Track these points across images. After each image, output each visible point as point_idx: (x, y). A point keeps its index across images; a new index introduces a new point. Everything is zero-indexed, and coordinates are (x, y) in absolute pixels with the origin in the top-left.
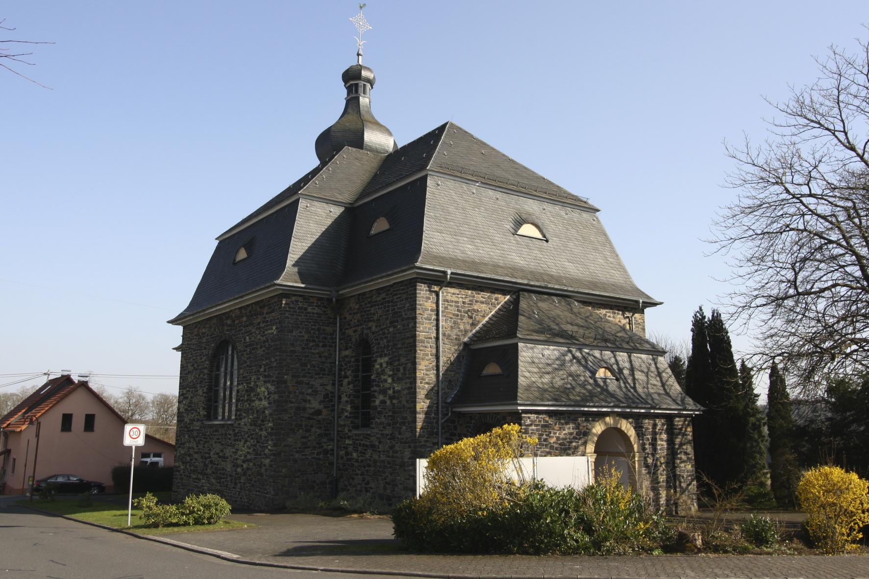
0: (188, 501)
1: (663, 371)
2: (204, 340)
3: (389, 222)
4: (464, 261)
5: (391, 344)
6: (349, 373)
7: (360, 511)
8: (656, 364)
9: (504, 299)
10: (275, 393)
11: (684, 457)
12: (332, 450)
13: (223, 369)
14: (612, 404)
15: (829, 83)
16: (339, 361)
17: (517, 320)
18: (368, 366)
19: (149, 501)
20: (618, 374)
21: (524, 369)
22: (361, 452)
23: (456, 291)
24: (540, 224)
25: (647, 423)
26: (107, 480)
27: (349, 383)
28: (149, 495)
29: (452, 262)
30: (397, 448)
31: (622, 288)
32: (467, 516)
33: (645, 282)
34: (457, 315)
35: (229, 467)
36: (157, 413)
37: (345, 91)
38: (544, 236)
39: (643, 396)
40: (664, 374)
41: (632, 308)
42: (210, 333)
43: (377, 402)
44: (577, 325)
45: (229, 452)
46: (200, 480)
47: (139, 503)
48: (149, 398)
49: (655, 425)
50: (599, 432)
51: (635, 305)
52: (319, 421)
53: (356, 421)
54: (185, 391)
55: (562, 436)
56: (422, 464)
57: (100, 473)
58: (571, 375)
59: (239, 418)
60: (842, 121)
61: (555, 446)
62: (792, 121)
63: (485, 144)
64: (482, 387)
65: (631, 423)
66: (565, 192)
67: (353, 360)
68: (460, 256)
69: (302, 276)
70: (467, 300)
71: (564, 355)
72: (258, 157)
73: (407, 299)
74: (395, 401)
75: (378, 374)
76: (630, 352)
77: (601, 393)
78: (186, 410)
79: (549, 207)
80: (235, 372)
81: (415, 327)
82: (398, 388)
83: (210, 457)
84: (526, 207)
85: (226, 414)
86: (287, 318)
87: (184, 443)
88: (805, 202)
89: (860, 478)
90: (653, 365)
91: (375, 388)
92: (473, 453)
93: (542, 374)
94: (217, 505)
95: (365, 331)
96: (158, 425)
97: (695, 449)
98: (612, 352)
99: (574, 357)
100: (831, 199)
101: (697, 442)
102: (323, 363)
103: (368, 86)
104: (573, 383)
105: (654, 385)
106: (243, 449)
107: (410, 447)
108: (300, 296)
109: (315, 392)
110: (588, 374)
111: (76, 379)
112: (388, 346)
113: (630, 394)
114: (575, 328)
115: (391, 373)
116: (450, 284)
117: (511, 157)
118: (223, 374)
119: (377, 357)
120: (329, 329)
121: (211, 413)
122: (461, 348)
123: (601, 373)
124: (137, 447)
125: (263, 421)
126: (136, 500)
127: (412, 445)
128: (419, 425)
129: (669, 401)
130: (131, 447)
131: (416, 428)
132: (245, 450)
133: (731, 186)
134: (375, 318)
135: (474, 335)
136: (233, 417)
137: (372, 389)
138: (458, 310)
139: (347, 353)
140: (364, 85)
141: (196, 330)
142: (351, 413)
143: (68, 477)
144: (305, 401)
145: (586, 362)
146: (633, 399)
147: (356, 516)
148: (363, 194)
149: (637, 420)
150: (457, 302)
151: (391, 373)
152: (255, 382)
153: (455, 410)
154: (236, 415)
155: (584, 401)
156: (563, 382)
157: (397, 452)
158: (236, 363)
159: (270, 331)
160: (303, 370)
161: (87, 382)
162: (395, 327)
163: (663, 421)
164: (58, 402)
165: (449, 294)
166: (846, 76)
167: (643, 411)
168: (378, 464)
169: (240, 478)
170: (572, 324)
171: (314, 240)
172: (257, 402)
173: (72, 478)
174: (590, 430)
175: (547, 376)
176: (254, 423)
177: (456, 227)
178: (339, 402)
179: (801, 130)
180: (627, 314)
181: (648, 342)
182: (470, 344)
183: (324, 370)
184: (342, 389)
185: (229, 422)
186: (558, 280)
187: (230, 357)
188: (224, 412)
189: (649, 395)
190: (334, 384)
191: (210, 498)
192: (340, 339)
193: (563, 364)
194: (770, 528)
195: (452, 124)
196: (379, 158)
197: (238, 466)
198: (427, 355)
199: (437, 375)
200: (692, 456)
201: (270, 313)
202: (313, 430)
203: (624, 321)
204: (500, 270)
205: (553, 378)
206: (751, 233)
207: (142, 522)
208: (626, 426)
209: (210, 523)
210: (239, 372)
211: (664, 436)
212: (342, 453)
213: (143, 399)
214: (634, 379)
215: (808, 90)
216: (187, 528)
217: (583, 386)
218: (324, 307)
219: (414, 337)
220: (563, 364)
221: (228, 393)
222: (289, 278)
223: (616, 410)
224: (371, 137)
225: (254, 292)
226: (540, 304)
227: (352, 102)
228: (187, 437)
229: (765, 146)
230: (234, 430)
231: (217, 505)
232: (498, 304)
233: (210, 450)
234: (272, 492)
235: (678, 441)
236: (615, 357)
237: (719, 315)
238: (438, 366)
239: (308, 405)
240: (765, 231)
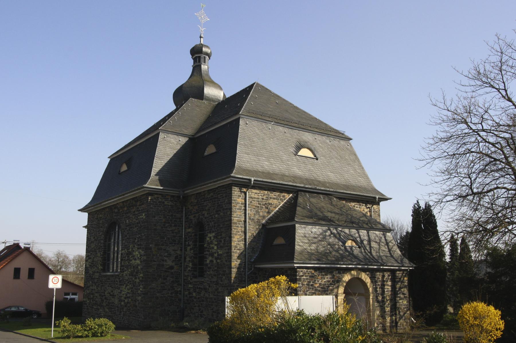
0: (88, 322)
1: (390, 242)
2: (101, 222)
3: (216, 147)
4: (263, 173)
5: (216, 225)
6: (191, 243)
7: (196, 329)
8: (385, 237)
9: (288, 197)
10: (144, 255)
11: (402, 296)
12: (181, 291)
13: (112, 240)
14: (355, 263)
15: (495, 59)
16: (185, 236)
17: (295, 210)
18: (202, 238)
19: (65, 322)
20: (360, 244)
21: (299, 241)
22: (198, 293)
23: (258, 191)
24: (313, 149)
25: (379, 275)
26: (43, 310)
27: (191, 249)
28: (65, 318)
29: (255, 173)
30: (220, 290)
31: (365, 189)
32: (253, 332)
33: (381, 185)
34: (258, 207)
35: (116, 301)
36: (76, 267)
37: (192, 61)
38: (315, 156)
39: (376, 257)
40: (390, 244)
41: (372, 202)
42: (105, 216)
43: (208, 262)
44: (334, 213)
45: (116, 292)
46: (99, 309)
47: (59, 323)
48: (71, 257)
49: (383, 276)
50: (347, 280)
51: (374, 200)
54: (89, 254)
55: (323, 283)
56: (228, 299)
57: (36, 305)
58: (329, 244)
59: (122, 271)
60: (504, 83)
61: (319, 289)
62: (472, 83)
63: (279, 97)
64: (273, 252)
65: (367, 275)
66: (331, 128)
67: (193, 235)
68: (260, 169)
69: (162, 182)
70: (264, 197)
71: (325, 232)
72: (136, 105)
73: (226, 196)
74: (218, 261)
75: (209, 244)
76: (368, 230)
77: (348, 256)
78: (90, 266)
79: (319, 137)
80: (120, 242)
81: (231, 214)
82: (220, 252)
83: (105, 296)
84: (304, 138)
85: (115, 268)
86: (152, 208)
88: (481, 135)
89: (496, 309)
90: (383, 238)
91: (207, 252)
92: (256, 293)
93: (311, 243)
94: (106, 325)
95: (201, 217)
96: (77, 274)
97: (409, 291)
98: (357, 230)
99: (332, 233)
100: (496, 133)
101: (411, 287)
103: (207, 58)
104: (331, 249)
105: (384, 251)
106: (125, 290)
107: (227, 289)
110: (341, 243)
111: (22, 246)
112: (215, 226)
113: (367, 256)
114: (333, 215)
115: (216, 243)
116: (254, 187)
117: (295, 105)
118: (112, 243)
119: (208, 233)
121: (106, 267)
122: (261, 227)
123: (349, 243)
124: (57, 289)
125: (137, 273)
126: (58, 322)
127: (229, 288)
128: (233, 275)
129: (392, 260)
130: (53, 289)
131: (231, 278)
133: (435, 124)
134: (207, 208)
135: (269, 219)
136: (119, 271)
137: (205, 253)
138: (259, 204)
139: (190, 230)
140: (205, 57)
142: (192, 268)
143: (18, 307)
144: (163, 261)
145: (340, 236)
146: (369, 259)
147: (193, 332)
148: (200, 129)
149: (372, 273)
150: (258, 198)
151: (216, 243)
152: (132, 249)
153: (256, 266)
154: (120, 269)
155: (337, 260)
156: (324, 249)
158: (120, 237)
159: (141, 217)
161: (29, 248)
162: (218, 214)
163: (389, 273)
164: (9, 262)
165: (253, 193)
166: (506, 54)
167: (375, 267)
168: (208, 300)
170: (331, 212)
171: (169, 159)
172: (133, 261)
173: (20, 308)
174: (341, 279)
175: (314, 245)
176: (131, 274)
177: (258, 150)
179: (478, 88)
180: (369, 206)
181: (380, 223)
182: (266, 225)
185: (117, 274)
186: (323, 184)
187: (117, 233)
188: (113, 267)
189: (380, 257)
190: (181, 250)
191: (103, 321)
192: (185, 222)
193: (324, 238)
194: (443, 340)
195: (258, 84)
196: (212, 106)
197: (122, 301)
198: (239, 232)
199: (245, 245)
200: (407, 295)
201: (141, 205)
202: (168, 278)
203: (366, 210)
204: (285, 178)
205: (318, 246)
206: (446, 154)
207: (60, 335)
208: (365, 277)
209: (102, 336)
210: (122, 242)
211: (389, 283)
212: (187, 293)
213: (67, 258)
214: (370, 247)
215: (483, 63)
216: (87, 338)
217: (337, 251)
219: (231, 220)
220: (324, 238)
221: (116, 255)
222: (153, 183)
223: (358, 266)
224: (208, 91)
225: (131, 192)
226: (312, 200)
227: (197, 68)
228: (91, 282)
229: (455, 99)
230: (119, 279)
231: (106, 325)
232: (284, 199)
233: (105, 291)
234: (143, 317)
235: (398, 286)
236: (358, 233)
238: (245, 239)
239: (165, 263)
240: (456, 153)
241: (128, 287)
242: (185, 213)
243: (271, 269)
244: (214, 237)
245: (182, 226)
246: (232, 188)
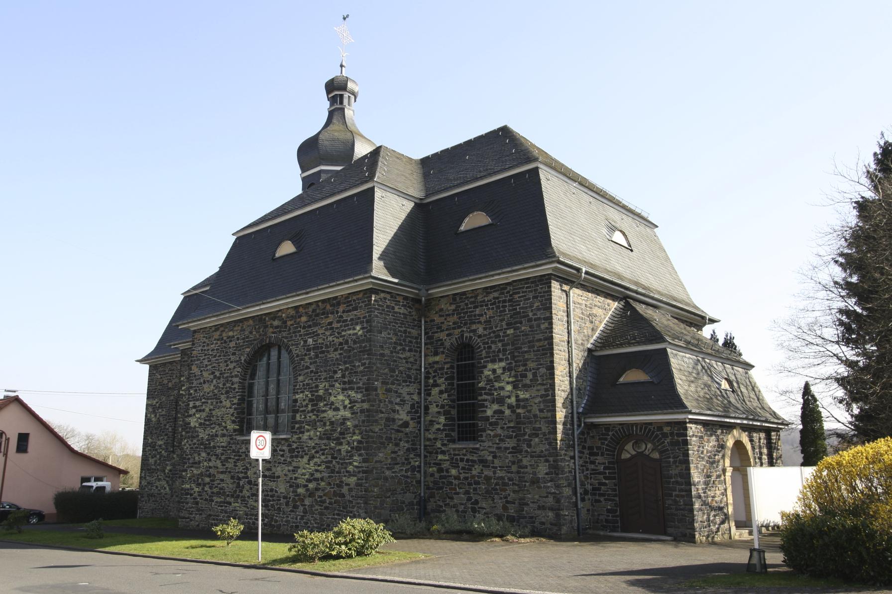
10: (363, 401)
12: (419, 467)
16: (425, 368)
27: (441, 392)
43: (489, 413)
46: (230, 503)
52: (406, 434)
53: (453, 434)
73: (535, 297)
83: (247, 477)
86: (377, 316)
87: (199, 462)
102: (409, 369)
103: (352, 97)
107: (547, 461)
108: (388, 293)
112: (505, 350)
119: (488, 362)
120: (414, 332)
122: (586, 354)
127: (551, 459)
128: (559, 436)
130: (257, 460)
132: (312, 467)
134: (483, 319)
141: (218, 333)
144: (394, 411)
147: (497, 539)
157: (526, 467)
160: (391, 376)
172: (331, 413)
178: (426, 413)
184: (429, 399)
190: (420, 394)
192: (425, 344)
197: (298, 486)
199: (571, 383)
202: (402, 444)
216: (349, 562)
218: (409, 307)
227: (336, 112)
233: (247, 469)
237: (732, 338)
239: (397, 416)
241: (315, 460)
243: (620, 424)
245: (421, 352)
246: (550, 283)
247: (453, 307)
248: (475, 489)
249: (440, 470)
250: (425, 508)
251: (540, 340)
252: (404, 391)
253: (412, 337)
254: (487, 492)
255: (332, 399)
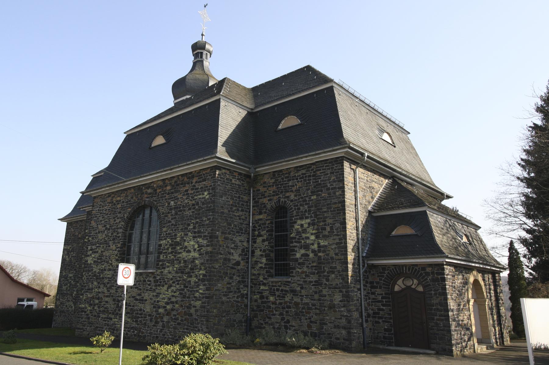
10: (208, 246)
12: (247, 294)
27: (263, 241)
35: (148, 308)
43: (298, 255)
46: (111, 319)
52: (238, 270)
53: (271, 271)
69: (230, 153)
78: (95, 262)
86: (219, 185)
87: (92, 289)
89: (511, 317)
103: (209, 54)
107: (341, 291)
109: (237, 247)
112: (310, 211)
119: (297, 219)
120: (246, 198)
127: (344, 290)
130: (123, 287)
132: (170, 293)
134: (294, 189)
141: (110, 198)
144: (230, 253)
147: (304, 351)
160: (229, 228)
169: (162, 318)
172: (184, 254)
178: (253, 256)
183: (242, 230)
190: (248, 242)
192: (253, 207)
197: (159, 308)
199: (357, 234)
202: (235, 277)
212: (257, 297)
218: (243, 180)
230: (155, 277)
239: (232, 257)
241: (172, 288)
242: (253, 196)
244: (309, 224)
245: (250, 212)
247: (273, 181)
248: (287, 312)
249: (262, 297)
250: (251, 325)
251: (335, 203)
252: (237, 239)
253: (244, 201)
254: (296, 314)
255: (186, 244)
